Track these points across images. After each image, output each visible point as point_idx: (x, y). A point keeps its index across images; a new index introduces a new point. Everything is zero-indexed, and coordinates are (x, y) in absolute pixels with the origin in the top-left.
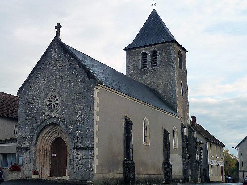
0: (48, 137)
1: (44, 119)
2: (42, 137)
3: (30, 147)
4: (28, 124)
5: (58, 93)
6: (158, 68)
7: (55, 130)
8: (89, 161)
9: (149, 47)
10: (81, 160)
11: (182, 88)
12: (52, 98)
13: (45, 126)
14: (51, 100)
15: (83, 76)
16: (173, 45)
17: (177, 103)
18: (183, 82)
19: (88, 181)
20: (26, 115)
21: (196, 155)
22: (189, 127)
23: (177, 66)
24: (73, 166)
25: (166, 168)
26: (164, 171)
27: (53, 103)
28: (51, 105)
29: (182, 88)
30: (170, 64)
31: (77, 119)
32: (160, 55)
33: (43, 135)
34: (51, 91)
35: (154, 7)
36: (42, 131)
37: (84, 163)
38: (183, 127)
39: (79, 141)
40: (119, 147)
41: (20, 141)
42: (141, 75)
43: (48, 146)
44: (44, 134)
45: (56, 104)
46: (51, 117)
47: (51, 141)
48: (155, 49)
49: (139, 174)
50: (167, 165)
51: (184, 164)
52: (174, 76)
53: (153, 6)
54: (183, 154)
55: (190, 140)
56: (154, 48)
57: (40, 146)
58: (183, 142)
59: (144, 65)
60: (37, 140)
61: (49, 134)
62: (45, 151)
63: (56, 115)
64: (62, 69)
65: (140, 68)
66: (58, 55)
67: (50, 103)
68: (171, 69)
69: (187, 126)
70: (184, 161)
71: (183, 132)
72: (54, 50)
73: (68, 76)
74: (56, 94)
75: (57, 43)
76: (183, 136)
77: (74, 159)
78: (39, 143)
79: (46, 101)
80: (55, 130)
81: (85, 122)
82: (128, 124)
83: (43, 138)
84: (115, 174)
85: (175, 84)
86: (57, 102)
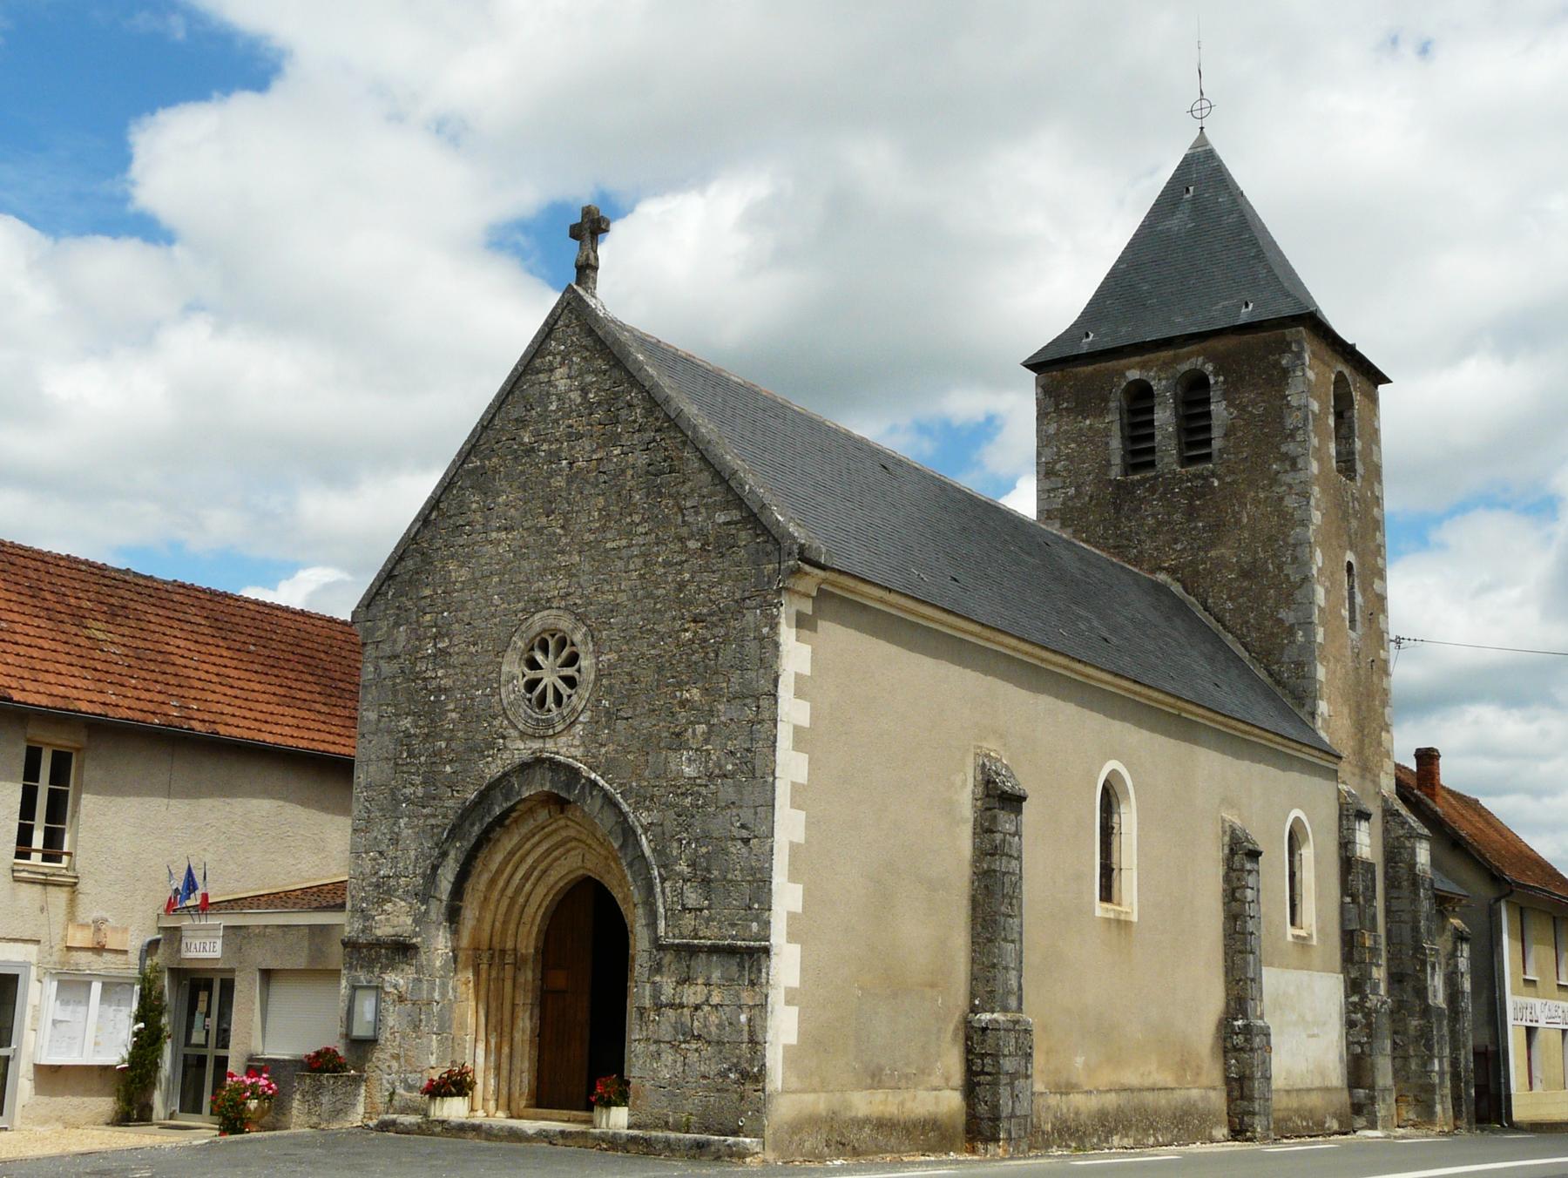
0: (526, 877)
1: (494, 770)
2: (486, 877)
3: (417, 935)
4: (407, 799)
5: (580, 618)
6: (1213, 474)
7: (564, 834)
8: (743, 1018)
10: (699, 1013)
11: (1352, 587)
12: (544, 649)
13: (506, 814)
14: (539, 657)
15: (721, 518)
16: (1299, 343)
17: (1321, 673)
18: (1356, 553)
20: (399, 742)
21: (1424, 971)
22: (1389, 813)
23: (1320, 460)
24: (653, 1048)
25: (1236, 1049)
26: (1227, 1068)
27: (550, 676)
28: (541, 687)
29: (1352, 587)
30: (1284, 449)
31: (680, 774)
32: (1226, 395)
33: (494, 867)
34: (539, 603)
35: (1198, 124)
36: (485, 840)
37: (713, 1029)
38: (1351, 813)
39: (692, 898)
40: (937, 934)
41: (363, 899)
42: (1118, 511)
43: (523, 930)
44: (499, 857)
45: (570, 682)
46: (538, 761)
47: (539, 899)
49: (1066, 1088)
50: (1240, 1039)
51: (1351, 1024)
52: (1305, 523)
54: (1345, 970)
55: (1392, 883)
57: (477, 929)
58: (1348, 899)
59: (1139, 452)
60: (458, 891)
61: (530, 861)
62: (509, 959)
63: (566, 749)
64: (603, 478)
65: (1115, 473)
66: (584, 391)
67: (531, 674)
68: (1287, 478)
69: (1374, 808)
70: (1351, 1008)
71: (1346, 844)
72: (562, 364)
73: (637, 518)
74: (566, 623)
75: (577, 329)
76: (1348, 862)
77: (659, 1007)
78: (470, 914)
79: (513, 666)
80: (564, 834)
81: (727, 791)
82: (1000, 798)
83: (493, 882)
84: (907, 1095)
85: (1307, 564)
86: (531, 674)
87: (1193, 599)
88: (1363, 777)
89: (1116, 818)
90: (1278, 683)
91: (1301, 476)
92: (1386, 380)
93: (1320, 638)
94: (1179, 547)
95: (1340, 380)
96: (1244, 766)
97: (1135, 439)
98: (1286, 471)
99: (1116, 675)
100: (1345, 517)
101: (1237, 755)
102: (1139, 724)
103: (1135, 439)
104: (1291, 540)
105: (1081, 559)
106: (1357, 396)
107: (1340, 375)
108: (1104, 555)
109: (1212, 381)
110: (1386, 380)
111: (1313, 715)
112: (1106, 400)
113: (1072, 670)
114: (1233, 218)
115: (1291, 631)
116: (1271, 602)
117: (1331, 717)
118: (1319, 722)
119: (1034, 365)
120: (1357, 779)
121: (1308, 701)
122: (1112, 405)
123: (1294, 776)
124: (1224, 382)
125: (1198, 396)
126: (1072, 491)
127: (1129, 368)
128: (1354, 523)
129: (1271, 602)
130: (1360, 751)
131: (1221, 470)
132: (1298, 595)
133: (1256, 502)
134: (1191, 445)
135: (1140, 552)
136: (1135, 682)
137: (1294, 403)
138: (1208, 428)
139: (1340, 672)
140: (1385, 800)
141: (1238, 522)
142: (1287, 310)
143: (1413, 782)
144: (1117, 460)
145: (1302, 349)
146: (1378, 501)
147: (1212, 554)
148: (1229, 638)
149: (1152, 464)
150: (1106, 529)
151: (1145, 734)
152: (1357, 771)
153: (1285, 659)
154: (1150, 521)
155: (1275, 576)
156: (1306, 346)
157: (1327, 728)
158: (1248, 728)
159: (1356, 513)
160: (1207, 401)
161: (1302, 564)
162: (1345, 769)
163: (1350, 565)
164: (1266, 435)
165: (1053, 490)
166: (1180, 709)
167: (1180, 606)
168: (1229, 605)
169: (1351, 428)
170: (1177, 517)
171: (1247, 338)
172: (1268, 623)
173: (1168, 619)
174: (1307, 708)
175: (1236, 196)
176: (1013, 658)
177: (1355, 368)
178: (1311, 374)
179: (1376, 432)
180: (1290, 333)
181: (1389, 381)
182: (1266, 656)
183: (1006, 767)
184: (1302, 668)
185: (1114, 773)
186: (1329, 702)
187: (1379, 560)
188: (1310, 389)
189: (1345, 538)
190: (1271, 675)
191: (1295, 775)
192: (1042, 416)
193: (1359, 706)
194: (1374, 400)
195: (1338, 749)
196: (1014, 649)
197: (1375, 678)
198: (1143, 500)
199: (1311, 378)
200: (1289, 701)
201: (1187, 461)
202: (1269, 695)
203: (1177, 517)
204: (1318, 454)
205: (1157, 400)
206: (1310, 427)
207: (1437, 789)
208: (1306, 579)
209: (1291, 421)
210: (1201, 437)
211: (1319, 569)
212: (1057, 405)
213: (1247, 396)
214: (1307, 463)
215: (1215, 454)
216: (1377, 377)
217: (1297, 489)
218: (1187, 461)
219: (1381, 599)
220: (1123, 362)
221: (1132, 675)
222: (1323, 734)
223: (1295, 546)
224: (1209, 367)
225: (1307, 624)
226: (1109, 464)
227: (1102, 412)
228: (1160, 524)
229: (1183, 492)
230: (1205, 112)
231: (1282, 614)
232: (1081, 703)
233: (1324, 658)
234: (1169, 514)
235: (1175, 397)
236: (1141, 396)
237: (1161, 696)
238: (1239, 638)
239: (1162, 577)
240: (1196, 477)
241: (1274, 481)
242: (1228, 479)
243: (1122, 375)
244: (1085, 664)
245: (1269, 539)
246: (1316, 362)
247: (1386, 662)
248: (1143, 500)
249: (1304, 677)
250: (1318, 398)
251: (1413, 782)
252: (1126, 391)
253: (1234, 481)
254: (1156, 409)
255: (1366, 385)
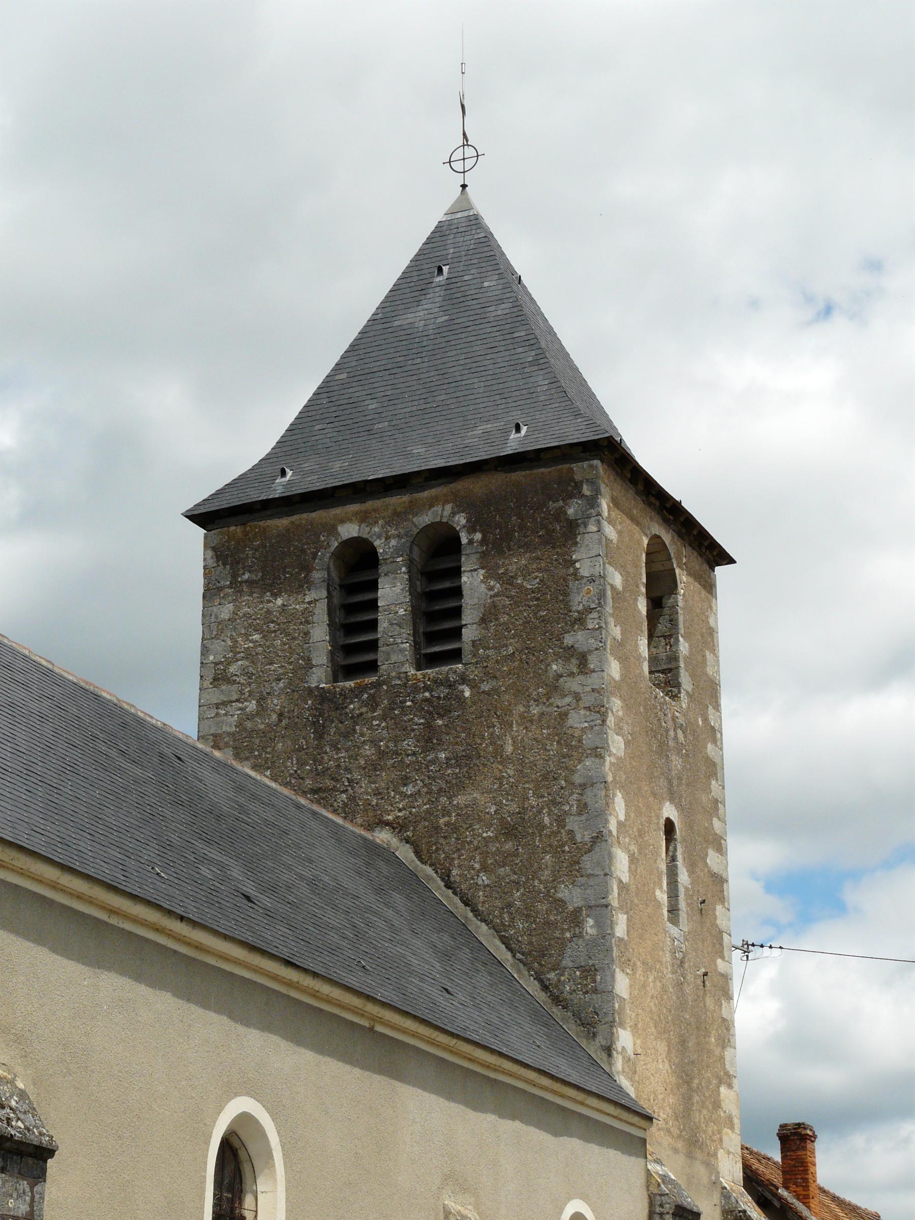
6: (464, 680)
9: (398, 501)
16: (593, 483)
17: (622, 985)
18: (680, 807)
19: (303, 801)
23: (623, 660)
30: (568, 640)
32: (485, 560)
42: (320, 736)
48: (442, 512)
52: (598, 752)
53: (458, 166)
56: (439, 510)
59: (355, 648)
65: (319, 678)
68: (573, 684)
85: (601, 815)
87: (429, 870)
88: (690, 1156)
89: (248, 1201)
90: (557, 1000)
91: (593, 680)
92: (728, 560)
93: (620, 929)
94: (409, 790)
95: (656, 550)
96: (485, 1123)
97: (350, 629)
98: (572, 674)
99: (253, 948)
100: (663, 750)
101: (477, 1106)
102: (297, 1039)
103: (350, 629)
104: (577, 779)
105: (240, 788)
106: (682, 577)
107: (655, 540)
108: (286, 791)
109: (464, 540)
110: (728, 560)
111: (608, 1050)
112: (307, 568)
113: (170, 935)
114: (502, 309)
115: (575, 918)
116: (546, 874)
117: (638, 1057)
118: (619, 1063)
119: (202, 517)
120: (681, 1159)
121: (601, 1028)
122: (318, 575)
123: (573, 1145)
124: (483, 541)
125: (446, 564)
126: (252, 706)
127: (342, 521)
128: (677, 762)
129: (546, 874)
130: (684, 1114)
131: (474, 673)
132: (587, 862)
133: (527, 721)
134: (432, 638)
135: (352, 799)
136: (288, 963)
137: (585, 572)
138: (457, 612)
139: (653, 988)
140: (725, 1194)
141: (498, 751)
142: (575, 433)
143: (776, 1178)
144: (321, 657)
145: (597, 493)
146: (714, 734)
147: (460, 800)
148: (482, 931)
149: (372, 667)
150: (301, 763)
151: (307, 1056)
152: (680, 1145)
153: (567, 962)
154: (368, 750)
155: (555, 833)
156: (603, 489)
157: (632, 1073)
158: (492, 1059)
159: (679, 747)
160: (457, 572)
161: (597, 816)
162: (659, 1137)
163: (669, 827)
164: (543, 620)
165: (224, 704)
166: (374, 1019)
167: (410, 882)
168: (484, 879)
169: (673, 622)
170: (409, 744)
171: (518, 476)
172: (542, 907)
173: (379, 891)
174: (600, 1040)
175: (511, 281)
176: (52, 902)
177: (680, 535)
178: (610, 532)
179: (711, 632)
180: (580, 469)
181: (732, 561)
182: (537, 958)
183: (23, 1095)
184: (593, 976)
185: (245, 1119)
186: (635, 1029)
187: (716, 823)
188: (610, 554)
189: (663, 782)
190: (545, 988)
191: (575, 1144)
192: (211, 593)
193: (683, 1042)
194: (710, 587)
195: (647, 1107)
196: (79, 897)
197: (709, 1002)
198: (357, 719)
199: (612, 545)
200: (572, 1028)
201: (426, 661)
202: (540, 1017)
203: (409, 744)
204: (621, 651)
205: (382, 569)
206: (609, 609)
207: (813, 1190)
208: (599, 838)
209: (579, 600)
210: (447, 625)
211: (620, 824)
212: (234, 576)
213: (515, 562)
214: (602, 661)
215: (467, 647)
216: (714, 554)
217: (588, 700)
218: (426, 661)
219: (719, 881)
220: (338, 511)
221: (285, 953)
222: (624, 1082)
223: (583, 786)
224: (461, 520)
225: (600, 908)
226: (309, 665)
227: (303, 585)
228: (382, 754)
229: (418, 707)
230: (469, 163)
231: (563, 892)
232: (187, 994)
233: (627, 963)
234: (396, 740)
235: (410, 563)
236: (360, 563)
237: (336, 993)
238: (498, 930)
239: (383, 836)
240: (437, 682)
241: (554, 688)
242: (485, 687)
243: (332, 530)
244: (194, 924)
245: (545, 777)
246: (616, 513)
247: (726, 978)
248: (357, 719)
249: (595, 991)
250: (622, 569)
251: (776, 1178)
252: (338, 555)
253: (495, 690)
254: (382, 582)
255: (697, 563)
